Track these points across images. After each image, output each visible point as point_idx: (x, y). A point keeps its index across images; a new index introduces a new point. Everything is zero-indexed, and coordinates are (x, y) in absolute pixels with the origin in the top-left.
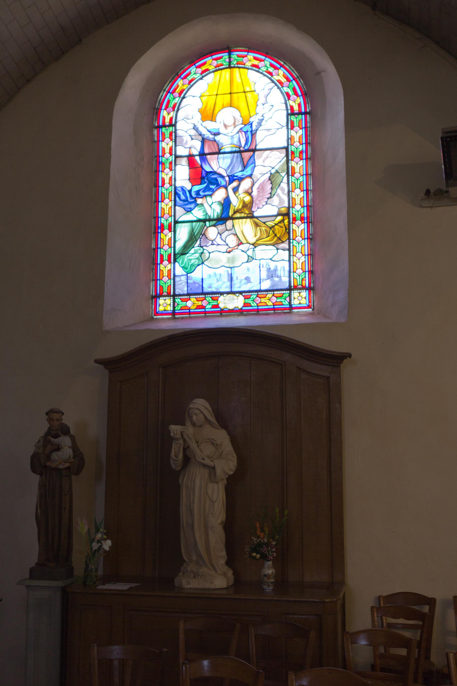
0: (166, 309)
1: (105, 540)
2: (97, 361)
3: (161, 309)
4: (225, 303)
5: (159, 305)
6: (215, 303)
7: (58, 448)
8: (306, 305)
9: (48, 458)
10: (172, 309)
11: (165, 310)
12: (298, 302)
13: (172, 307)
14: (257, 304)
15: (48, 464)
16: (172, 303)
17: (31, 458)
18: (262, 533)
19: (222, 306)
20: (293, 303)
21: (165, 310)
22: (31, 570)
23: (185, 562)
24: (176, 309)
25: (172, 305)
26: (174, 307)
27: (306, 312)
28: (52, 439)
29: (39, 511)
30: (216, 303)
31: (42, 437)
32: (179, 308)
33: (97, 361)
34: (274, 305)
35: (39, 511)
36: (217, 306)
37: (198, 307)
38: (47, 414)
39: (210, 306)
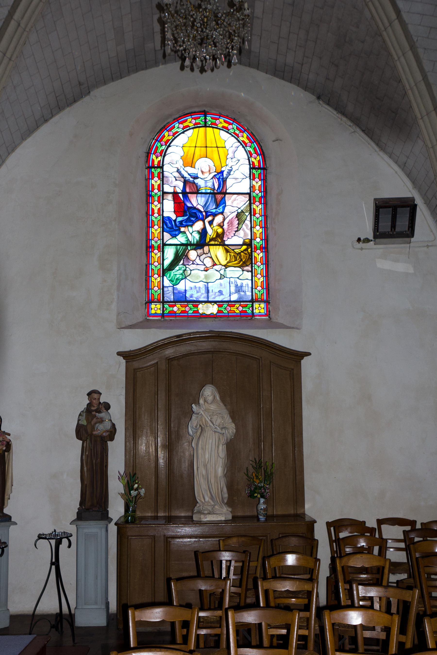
0: (157, 312)
2: (119, 354)
3: (153, 312)
4: (203, 310)
5: (152, 309)
7: (101, 421)
11: (156, 313)
14: (228, 311)
19: (201, 311)
21: (156, 313)
23: (198, 503)
26: (163, 311)
28: (97, 414)
31: (83, 411)
33: (119, 354)
34: (228, 313)
36: (197, 312)
37: (183, 312)
38: (89, 394)
39: (192, 311)
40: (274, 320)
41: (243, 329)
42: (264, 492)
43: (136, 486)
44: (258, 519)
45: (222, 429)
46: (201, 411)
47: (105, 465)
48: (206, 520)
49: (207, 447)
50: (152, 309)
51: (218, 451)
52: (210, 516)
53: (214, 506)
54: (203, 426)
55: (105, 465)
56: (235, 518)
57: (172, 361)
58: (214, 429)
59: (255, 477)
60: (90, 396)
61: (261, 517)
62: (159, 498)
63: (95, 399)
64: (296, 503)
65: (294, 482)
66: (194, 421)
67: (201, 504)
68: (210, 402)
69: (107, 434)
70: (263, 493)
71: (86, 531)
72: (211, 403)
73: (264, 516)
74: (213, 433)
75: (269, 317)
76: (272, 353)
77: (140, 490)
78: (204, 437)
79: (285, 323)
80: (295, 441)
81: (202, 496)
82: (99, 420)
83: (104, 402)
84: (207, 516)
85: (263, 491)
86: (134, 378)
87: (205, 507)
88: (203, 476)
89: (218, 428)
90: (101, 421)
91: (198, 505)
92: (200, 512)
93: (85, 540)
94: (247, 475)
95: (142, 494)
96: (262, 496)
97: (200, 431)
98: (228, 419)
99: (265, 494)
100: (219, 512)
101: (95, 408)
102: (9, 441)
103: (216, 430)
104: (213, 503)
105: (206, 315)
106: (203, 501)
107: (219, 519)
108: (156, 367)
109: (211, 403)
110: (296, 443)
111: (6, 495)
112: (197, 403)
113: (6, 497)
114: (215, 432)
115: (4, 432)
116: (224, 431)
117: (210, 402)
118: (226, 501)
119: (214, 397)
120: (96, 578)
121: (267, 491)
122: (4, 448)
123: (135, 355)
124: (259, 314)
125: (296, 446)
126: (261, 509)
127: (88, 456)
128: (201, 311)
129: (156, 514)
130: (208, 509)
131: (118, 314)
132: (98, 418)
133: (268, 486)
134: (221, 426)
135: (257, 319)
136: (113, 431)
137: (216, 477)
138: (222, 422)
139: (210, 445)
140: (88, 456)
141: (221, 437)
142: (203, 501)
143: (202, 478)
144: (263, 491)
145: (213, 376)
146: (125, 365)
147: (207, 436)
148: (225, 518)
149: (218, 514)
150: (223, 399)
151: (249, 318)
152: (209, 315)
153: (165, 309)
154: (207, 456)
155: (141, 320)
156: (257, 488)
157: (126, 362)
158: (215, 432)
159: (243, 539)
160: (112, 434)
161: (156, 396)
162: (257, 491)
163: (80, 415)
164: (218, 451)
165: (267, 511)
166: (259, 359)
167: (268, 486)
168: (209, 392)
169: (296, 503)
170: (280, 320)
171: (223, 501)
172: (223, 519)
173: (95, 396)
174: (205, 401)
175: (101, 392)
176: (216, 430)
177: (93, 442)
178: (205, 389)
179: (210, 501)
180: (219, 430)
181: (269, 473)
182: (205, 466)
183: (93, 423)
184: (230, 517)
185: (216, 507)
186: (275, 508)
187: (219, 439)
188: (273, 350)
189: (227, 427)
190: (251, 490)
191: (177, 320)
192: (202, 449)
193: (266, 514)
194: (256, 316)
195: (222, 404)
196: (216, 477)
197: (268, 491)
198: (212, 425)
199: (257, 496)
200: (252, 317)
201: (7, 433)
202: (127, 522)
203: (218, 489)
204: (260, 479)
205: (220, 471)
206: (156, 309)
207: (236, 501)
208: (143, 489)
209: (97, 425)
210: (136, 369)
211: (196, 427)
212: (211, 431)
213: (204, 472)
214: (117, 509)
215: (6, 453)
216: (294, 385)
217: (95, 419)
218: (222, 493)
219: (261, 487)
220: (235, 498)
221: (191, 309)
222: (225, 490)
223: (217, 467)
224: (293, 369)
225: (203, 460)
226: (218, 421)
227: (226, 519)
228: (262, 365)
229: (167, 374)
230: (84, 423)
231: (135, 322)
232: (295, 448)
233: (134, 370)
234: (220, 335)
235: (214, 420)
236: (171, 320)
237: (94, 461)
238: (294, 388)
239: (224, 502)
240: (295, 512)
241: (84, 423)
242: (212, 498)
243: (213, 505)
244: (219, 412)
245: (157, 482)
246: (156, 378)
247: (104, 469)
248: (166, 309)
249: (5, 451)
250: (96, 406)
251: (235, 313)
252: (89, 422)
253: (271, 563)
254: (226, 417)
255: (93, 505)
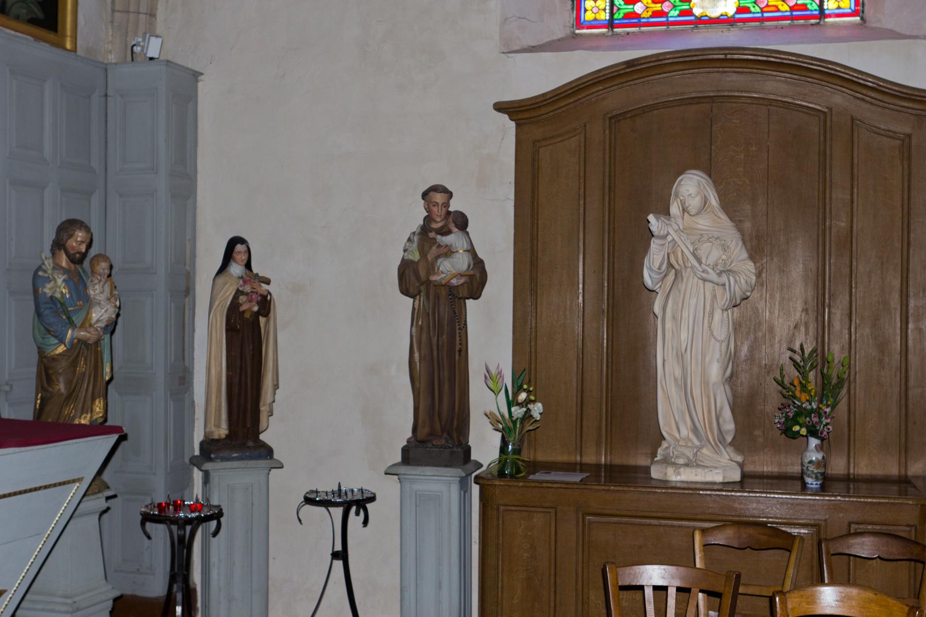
0: (598, 17)
1: (534, 402)
2: (500, 107)
3: (589, 16)
4: (703, 8)
5: (586, 10)
6: (685, 7)
7: (448, 252)
8: (849, 11)
9: (432, 268)
10: (608, 18)
11: (595, 19)
12: (835, 6)
13: (608, 15)
14: (762, 9)
15: (434, 278)
16: (608, 8)
17: (399, 269)
18: (803, 394)
19: (697, 11)
20: (825, 7)
21: (595, 19)
22: (405, 451)
23: (664, 439)
24: (616, 16)
25: (608, 11)
26: (612, 14)
27: (849, 22)
28: (439, 237)
29: (417, 355)
30: (687, 7)
31: (414, 233)
32: (621, 15)
33: (500, 107)
34: (762, 12)
35: (417, 355)
36: (689, 12)
37: (656, 14)
38: (425, 195)
39: (677, 12)
40: (873, 22)
41: (789, 43)
42: (817, 423)
43: (523, 396)
44: (804, 487)
45: (719, 274)
46: (672, 232)
47: (457, 349)
48: (679, 478)
49: (685, 314)
50: (586, 10)
51: (710, 324)
52: (688, 470)
53: (699, 449)
54: (677, 267)
55: (457, 349)
56: (748, 480)
57: (619, 121)
58: (700, 274)
59: (798, 388)
60: (427, 197)
61: (809, 480)
62: (584, 423)
63: (437, 203)
64: (906, 451)
65: (903, 402)
66: (655, 256)
67: (673, 442)
68: (693, 212)
69: (462, 281)
70: (814, 426)
71: (418, 487)
72: (697, 214)
73: (817, 478)
74: (701, 282)
75: (862, 18)
76: (858, 98)
77: (530, 406)
78: (679, 291)
79: (898, 29)
80: (907, 306)
81: (674, 426)
82: (443, 250)
83: (456, 212)
84: (682, 470)
85: (815, 420)
86: (533, 160)
87: (681, 449)
88: (676, 380)
89: (710, 271)
90: (448, 252)
91: (665, 445)
92: (666, 461)
93: (416, 506)
94: (781, 384)
95: (537, 416)
96: (813, 432)
97: (671, 277)
98: (738, 253)
99: (820, 428)
100: (710, 464)
101: (440, 225)
102: (266, 293)
103: (704, 275)
104: (697, 442)
105: (711, 18)
106: (677, 435)
107: (709, 478)
108: (583, 135)
109: (697, 214)
110: (911, 312)
111: (261, 404)
112: (665, 211)
113: (264, 409)
114: (704, 280)
115: (257, 274)
116: (724, 278)
117: (693, 212)
118: (729, 439)
119: (705, 201)
120: (439, 586)
121: (825, 421)
122: (256, 309)
123: (824, 230)
124: (837, 11)
125: (911, 319)
126: (811, 462)
127: (421, 328)
128: (697, 11)
129: (578, 458)
130: (683, 454)
131: (505, 20)
132: (439, 246)
133: (828, 410)
134: (720, 268)
135: (833, 25)
136: (478, 275)
137: (705, 382)
138: (724, 257)
139: (692, 310)
140: (421, 328)
141: (719, 291)
142: (677, 435)
143: (673, 384)
144: (815, 420)
145: (713, 154)
146: (514, 133)
147: (685, 290)
148: (724, 478)
149: (707, 467)
150: (728, 206)
151: (813, 21)
152: (718, 18)
153: (615, 8)
154: (684, 336)
155: (560, 35)
156: (801, 412)
157: (518, 126)
158: (704, 280)
159: (751, 531)
160: (476, 280)
161: (582, 202)
162: (801, 420)
163: (409, 240)
164: (710, 324)
165: (825, 466)
166: (824, 113)
167: (828, 410)
168: (692, 187)
169: (906, 451)
170: (888, 23)
171: (722, 439)
172: (719, 478)
173: (439, 198)
174: (684, 210)
175: (450, 189)
176: (704, 275)
177: (431, 297)
178: (681, 180)
179: (692, 436)
180: (713, 276)
181: (834, 381)
182: (680, 356)
183: (430, 257)
184: (736, 476)
185: (704, 451)
186: (852, 460)
187: (714, 297)
188: (859, 89)
189: (735, 269)
190: (787, 417)
191: (642, 32)
192: (674, 318)
193: (823, 474)
194: (829, 16)
195: (723, 216)
196: (705, 382)
197: (829, 421)
198: (697, 264)
199: (798, 432)
200: (820, 19)
201: (262, 277)
202: (501, 474)
203: (709, 411)
204: (810, 391)
205: (715, 372)
206: (595, 10)
207: (761, 440)
208: (539, 405)
209: (440, 261)
210: (539, 141)
211: (659, 269)
212: (696, 279)
213: (678, 372)
214: (485, 446)
215: (262, 320)
216: (910, 174)
217: (434, 248)
218: (721, 420)
219: (812, 411)
220: (757, 433)
221: (675, 6)
222: (727, 413)
223: (707, 359)
224: (909, 136)
225: (675, 346)
226: (713, 255)
227: (726, 481)
228: (831, 127)
229: (608, 151)
230: (416, 257)
231: (545, 39)
232: (907, 323)
233: (535, 142)
234: (729, 57)
235: (702, 253)
236: (628, 33)
237: (435, 340)
238: (909, 181)
239: (724, 439)
240: (903, 472)
241: (416, 257)
242: (695, 430)
243: (696, 447)
244: (716, 234)
245: (582, 391)
246: (582, 160)
247: (457, 357)
248: (619, 9)
249: (258, 314)
250: (438, 220)
251: (778, 10)
252: (423, 252)
253: (790, 606)
254: (732, 246)
255: (438, 435)
